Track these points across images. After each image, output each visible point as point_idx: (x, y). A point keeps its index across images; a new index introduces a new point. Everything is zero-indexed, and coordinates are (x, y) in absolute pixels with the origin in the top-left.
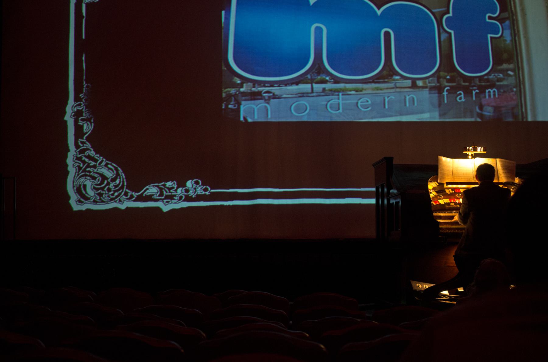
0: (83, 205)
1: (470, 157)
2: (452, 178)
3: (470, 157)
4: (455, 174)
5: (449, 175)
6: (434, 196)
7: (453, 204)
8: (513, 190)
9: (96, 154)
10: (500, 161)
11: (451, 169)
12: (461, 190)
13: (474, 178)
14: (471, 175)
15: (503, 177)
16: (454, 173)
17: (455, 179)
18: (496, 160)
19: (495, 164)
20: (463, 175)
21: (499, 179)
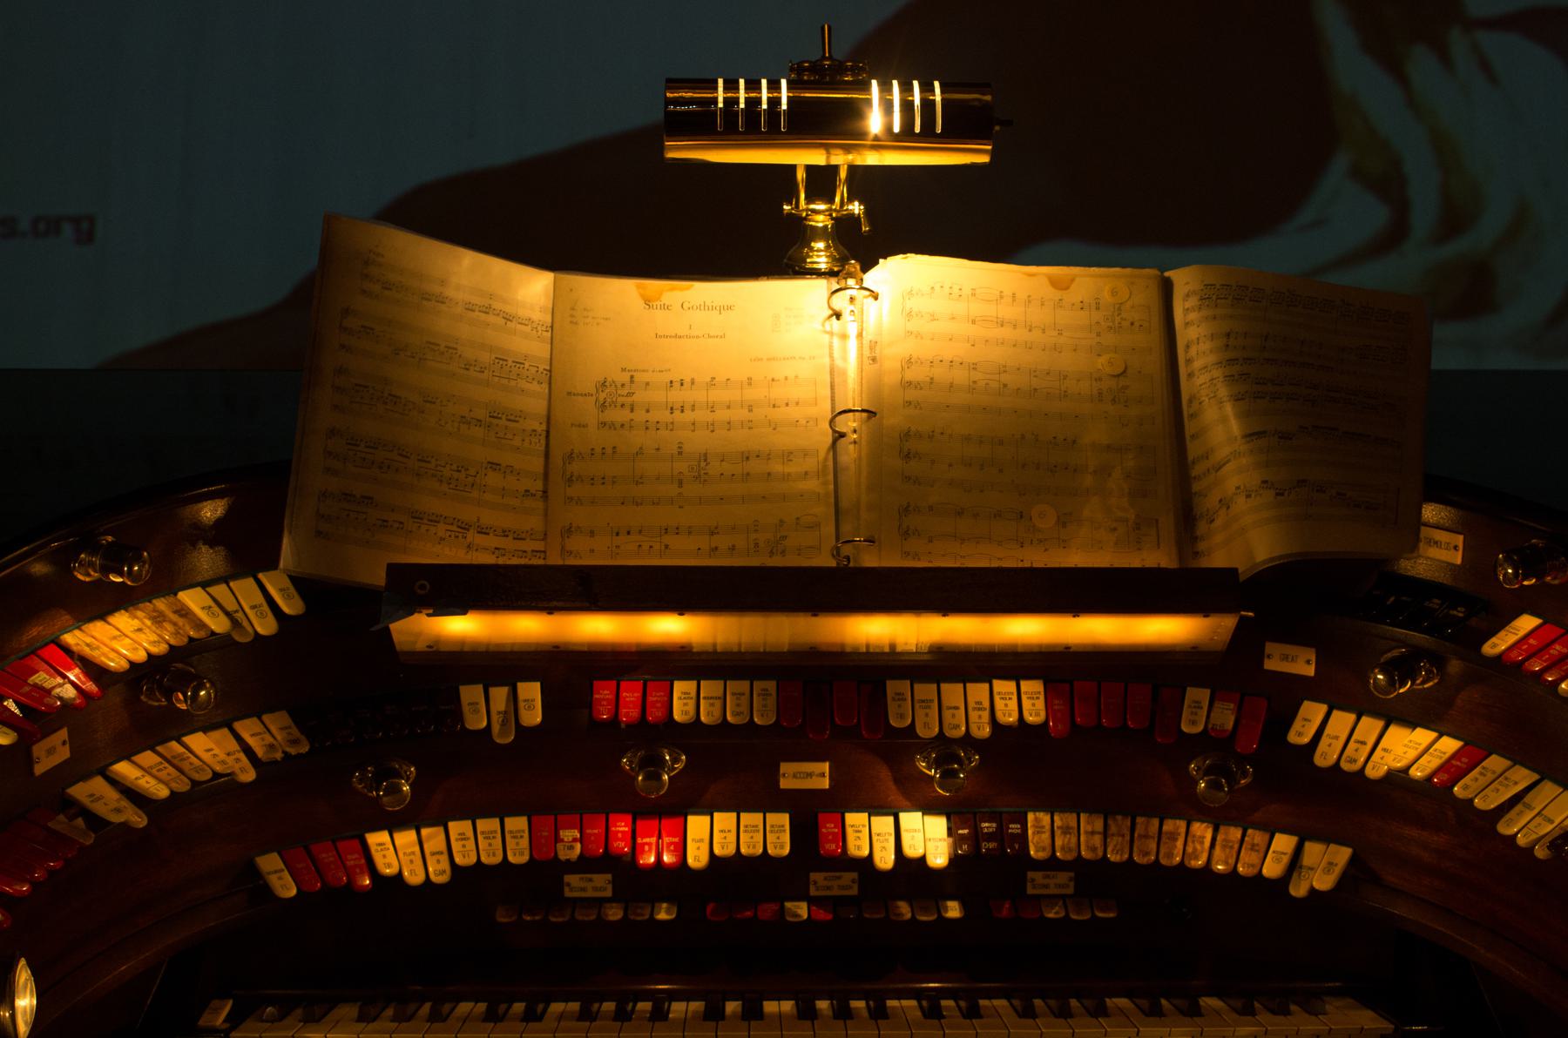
0: (257, 615)
1: (820, 256)
2: (535, 522)
3: (820, 256)
4: (576, 467)
5: (493, 479)
6: (249, 775)
7: (600, 884)
8: (1391, 683)
9: (831, 200)
10: (1209, 297)
11: (533, 401)
12: (471, 694)
13: (508, 543)
14: (812, 485)
15: (1241, 504)
16: (570, 457)
17: (568, 531)
18: (1167, 288)
19: (1155, 337)
20: (700, 477)
21: (1202, 527)
